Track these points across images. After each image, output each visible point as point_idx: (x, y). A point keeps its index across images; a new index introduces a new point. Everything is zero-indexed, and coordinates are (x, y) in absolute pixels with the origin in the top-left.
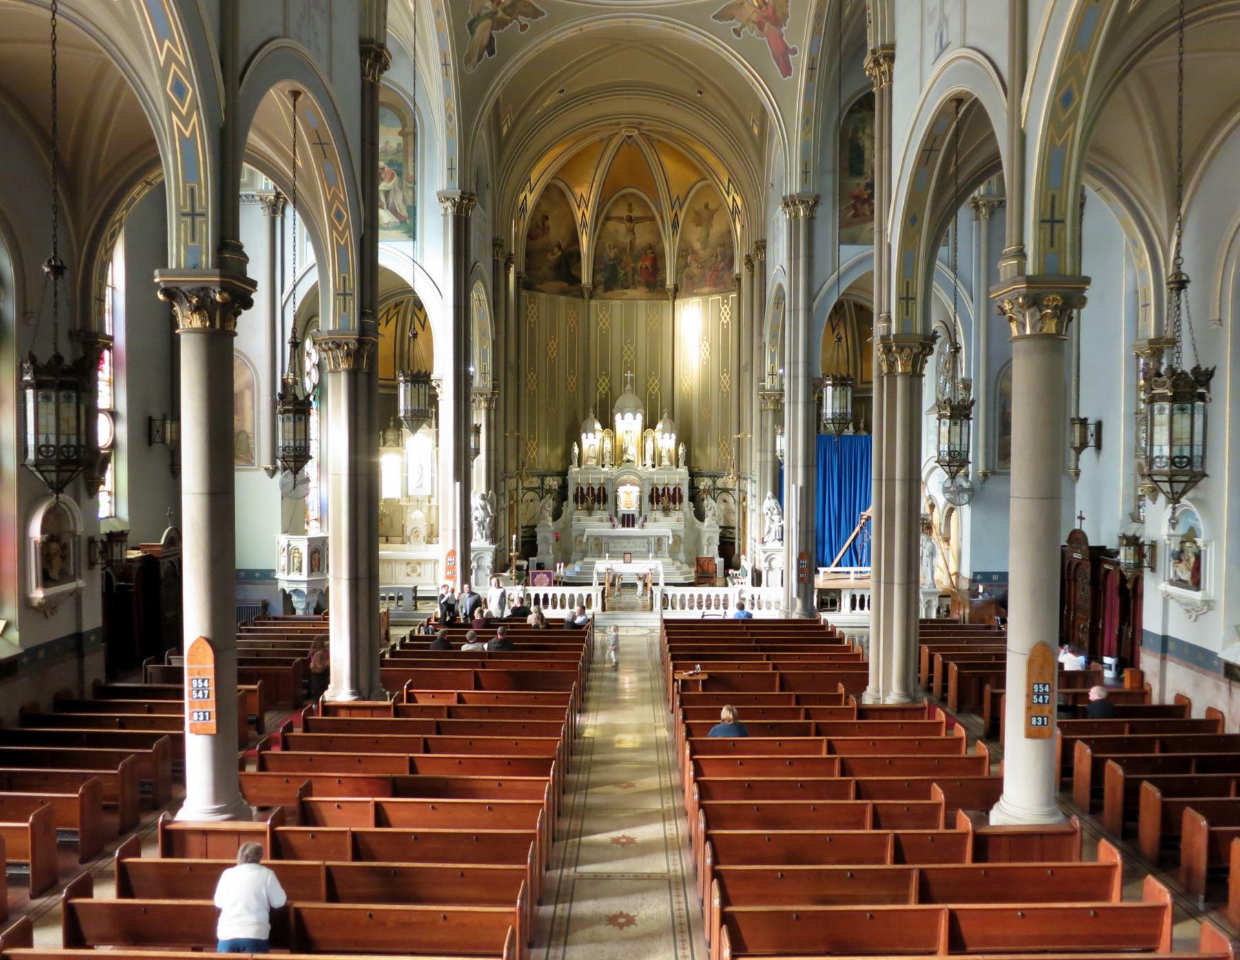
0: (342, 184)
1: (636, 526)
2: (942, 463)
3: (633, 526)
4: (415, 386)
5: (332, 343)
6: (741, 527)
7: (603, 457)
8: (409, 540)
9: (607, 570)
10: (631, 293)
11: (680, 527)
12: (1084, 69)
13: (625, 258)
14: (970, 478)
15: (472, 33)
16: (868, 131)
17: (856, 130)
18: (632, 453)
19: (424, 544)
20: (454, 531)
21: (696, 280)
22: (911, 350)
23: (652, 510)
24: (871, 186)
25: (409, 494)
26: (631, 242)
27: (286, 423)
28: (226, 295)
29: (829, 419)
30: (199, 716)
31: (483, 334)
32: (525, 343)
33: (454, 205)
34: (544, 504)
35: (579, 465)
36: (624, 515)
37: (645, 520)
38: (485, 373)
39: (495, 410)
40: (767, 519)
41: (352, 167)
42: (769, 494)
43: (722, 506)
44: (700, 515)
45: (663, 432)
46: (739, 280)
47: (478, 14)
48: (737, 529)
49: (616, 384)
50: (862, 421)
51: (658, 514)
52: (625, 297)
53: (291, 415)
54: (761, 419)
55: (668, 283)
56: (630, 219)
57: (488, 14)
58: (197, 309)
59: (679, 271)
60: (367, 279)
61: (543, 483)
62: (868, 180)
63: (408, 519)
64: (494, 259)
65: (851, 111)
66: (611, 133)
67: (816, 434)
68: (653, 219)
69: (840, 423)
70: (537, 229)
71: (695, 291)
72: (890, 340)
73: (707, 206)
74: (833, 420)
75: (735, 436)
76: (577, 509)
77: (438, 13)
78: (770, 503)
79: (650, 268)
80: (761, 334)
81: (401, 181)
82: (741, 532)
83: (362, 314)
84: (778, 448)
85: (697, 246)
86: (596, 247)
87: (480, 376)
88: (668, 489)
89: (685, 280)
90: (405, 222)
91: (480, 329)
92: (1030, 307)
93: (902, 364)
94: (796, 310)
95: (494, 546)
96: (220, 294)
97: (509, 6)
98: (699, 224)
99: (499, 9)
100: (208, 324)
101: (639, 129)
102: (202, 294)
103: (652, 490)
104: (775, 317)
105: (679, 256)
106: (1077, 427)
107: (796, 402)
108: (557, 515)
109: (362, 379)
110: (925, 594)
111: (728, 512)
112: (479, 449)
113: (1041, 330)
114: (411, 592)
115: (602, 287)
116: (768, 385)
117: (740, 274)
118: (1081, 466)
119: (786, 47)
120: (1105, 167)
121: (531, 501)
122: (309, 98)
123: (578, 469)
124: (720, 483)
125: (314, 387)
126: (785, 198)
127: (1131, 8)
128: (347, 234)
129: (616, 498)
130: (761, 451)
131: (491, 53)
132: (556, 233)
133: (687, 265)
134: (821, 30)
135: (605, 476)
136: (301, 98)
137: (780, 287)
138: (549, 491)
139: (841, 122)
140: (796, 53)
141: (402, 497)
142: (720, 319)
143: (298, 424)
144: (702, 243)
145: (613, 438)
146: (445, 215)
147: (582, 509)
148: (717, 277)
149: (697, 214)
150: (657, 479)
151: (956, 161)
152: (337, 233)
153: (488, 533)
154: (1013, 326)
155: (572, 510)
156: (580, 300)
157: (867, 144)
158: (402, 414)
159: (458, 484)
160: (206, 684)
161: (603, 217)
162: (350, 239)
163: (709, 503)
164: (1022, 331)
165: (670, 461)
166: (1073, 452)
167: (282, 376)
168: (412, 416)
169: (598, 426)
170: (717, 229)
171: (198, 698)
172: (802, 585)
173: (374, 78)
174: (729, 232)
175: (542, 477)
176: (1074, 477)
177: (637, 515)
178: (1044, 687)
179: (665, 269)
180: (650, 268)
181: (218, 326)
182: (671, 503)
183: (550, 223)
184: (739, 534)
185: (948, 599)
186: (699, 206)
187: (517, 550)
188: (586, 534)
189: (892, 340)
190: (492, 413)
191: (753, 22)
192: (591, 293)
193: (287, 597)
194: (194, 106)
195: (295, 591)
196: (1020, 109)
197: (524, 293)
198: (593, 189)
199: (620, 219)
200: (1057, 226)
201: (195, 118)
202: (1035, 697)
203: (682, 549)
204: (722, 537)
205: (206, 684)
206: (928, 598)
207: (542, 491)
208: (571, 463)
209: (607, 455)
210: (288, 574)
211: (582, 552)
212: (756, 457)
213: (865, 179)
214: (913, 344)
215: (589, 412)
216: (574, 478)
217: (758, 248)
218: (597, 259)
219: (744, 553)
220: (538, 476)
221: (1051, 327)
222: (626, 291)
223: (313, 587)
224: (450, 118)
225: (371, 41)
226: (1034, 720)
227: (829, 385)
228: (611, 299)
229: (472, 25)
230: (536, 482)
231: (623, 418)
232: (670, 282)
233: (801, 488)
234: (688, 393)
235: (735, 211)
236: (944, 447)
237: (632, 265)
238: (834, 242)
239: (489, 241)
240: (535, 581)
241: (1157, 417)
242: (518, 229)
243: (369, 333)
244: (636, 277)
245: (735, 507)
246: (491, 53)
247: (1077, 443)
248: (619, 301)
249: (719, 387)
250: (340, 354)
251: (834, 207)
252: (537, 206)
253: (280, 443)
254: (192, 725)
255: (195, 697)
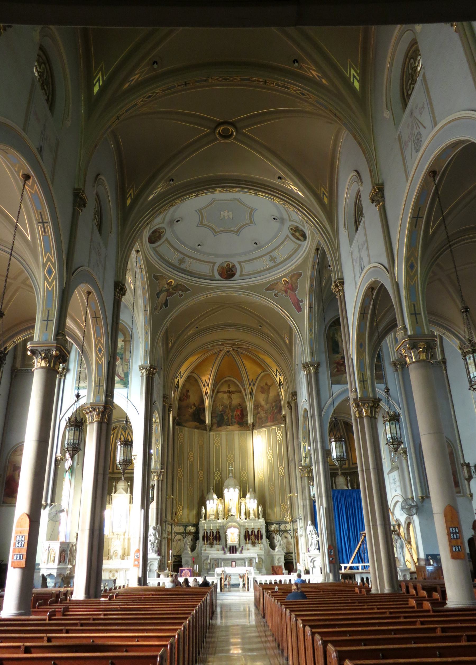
0: (103, 336)
1: (237, 552)
2: (389, 444)
3: (236, 553)
4: (125, 447)
5: (92, 408)
6: (296, 551)
7: (218, 513)
8: (112, 558)
9: (223, 571)
10: (230, 428)
11: (262, 553)
12: (416, 255)
13: (227, 411)
14: (415, 499)
15: (158, 297)
16: (339, 334)
17: (334, 334)
18: (234, 511)
19: (120, 560)
20: (140, 538)
21: (263, 419)
22: (369, 404)
23: (246, 544)
24: (343, 358)
25: (113, 531)
26: (230, 403)
27: (70, 432)
28: (58, 352)
29: (335, 458)
30: (17, 557)
31: (157, 440)
32: (177, 452)
33: (146, 371)
34: (186, 541)
35: (205, 519)
36: (230, 546)
37: (242, 549)
38: (157, 461)
39: (162, 481)
40: (309, 537)
41: (108, 332)
42: (310, 522)
43: (285, 541)
44: (273, 546)
45: (250, 499)
46: (285, 417)
47: (161, 290)
48: (294, 553)
49: (224, 476)
50: (355, 484)
51: (249, 546)
52: (227, 430)
53: (73, 428)
54: (302, 483)
55: (249, 422)
56: (229, 392)
57: (165, 290)
58: (44, 358)
59: (254, 416)
60: (110, 380)
61: (185, 530)
62: (342, 355)
63: (112, 545)
64: (163, 404)
65: (331, 326)
66: (220, 349)
67: (331, 489)
68: (240, 392)
69: (341, 460)
70: (184, 396)
71: (263, 425)
72: (358, 400)
73: (267, 384)
74: (337, 459)
75: (289, 495)
76: (204, 544)
77: (144, 288)
78: (310, 528)
79: (240, 415)
80: (298, 438)
81: (122, 361)
82: (296, 555)
83: (107, 396)
84: (312, 493)
85: (263, 403)
86: (213, 406)
87: (155, 462)
88: (254, 532)
89: (257, 420)
90: (123, 380)
91: (155, 438)
92: (412, 349)
93: (365, 411)
94: (314, 416)
95: (159, 557)
96: (55, 351)
97: (175, 287)
98: (263, 393)
99: (170, 288)
100: (48, 365)
101: (233, 347)
102: (47, 352)
103: (246, 532)
104: (304, 427)
105: (254, 409)
106: (465, 468)
107: (318, 462)
108: (193, 549)
109: (104, 426)
110: (402, 571)
111: (288, 543)
112: (153, 498)
113: (419, 358)
114: (112, 582)
115: (216, 425)
116: (303, 463)
117: (285, 415)
118: (472, 492)
119: (298, 300)
120: (444, 323)
121: (179, 540)
122: (94, 294)
123: (205, 521)
124: (282, 527)
125: (69, 468)
126: (303, 364)
127: (430, 233)
128: (103, 359)
129: (226, 537)
130: (303, 500)
131: (166, 306)
132: (193, 399)
133: (258, 413)
134: (313, 291)
135: (220, 525)
136: (90, 296)
137: (306, 409)
138: (189, 533)
139: (327, 331)
140: (303, 302)
141: (110, 533)
142: (277, 438)
143: (76, 432)
144: (265, 401)
145: (223, 503)
146: (142, 376)
147: (207, 544)
148: (273, 417)
149: (262, 388)
150: (248, 526)
151: (376, 320)
152: (98, 358)
153: (156, 549)
154: (407, 359)
155: (202, 545)
156: (205, 432)
157: (340, 340)
158: (118, 461)
159: (143, 510)
160: (23, 539)
161: (216, 391)
162: (104, 361)
163: (277, 538)
164: (411, 360)
165: (255, 515)
166: (466, 482)
167: (56, 455)
168: (123, 462)
169: (215, 496)
170: (272, 394)
171: (18, 546)
172: (332, 565)
173: (119, 297)
174: (278, 395)
175: (185, 526)
176: (470, 498)
177: (237, 546)
178: (455, 529)
179: (247, 415)
180: (240, 415)
181: (52, 366)
182: (256, 540)
183: (190, 394)
184: (295, 557)
185: (416, 574)
186: (263, 384)
187: (171, 560)
188: (210, 558)
189: (359, 400)
190: (160, 482)
191: (283, 291)
192: (210, 428)
193: (44, 579)
194: (55, 278)
195: (50, 575)
196: (394, 274)
197: (177, 427)
198: (211, 377)
199: (224, 392)
200: (418, 316)
201: (54, 283)
202: (452, 535)
203: (264, 566)
204: (286, 559)
205: (23, 539)
206: (404, 574)
207: (185, 533)
208: (201, 518)
209: (221, 513)
210: (47, 564)
211: (207, 570)
212: (301, 503)
213: (341, 355)
214: (369, 402)
215: (210, 489)
216: (203, 527)
217: (293, 396)
218: (213, 412)
219: (299, 562)
220: (183, 526)
221: (423, 356)
222: (228, 427)
223: (60, 572)
224: (147, 333)
225: (119, 282)
226: (454, 548)
227: (333, 441)
228: (221, 431)
229: (158, 295)
230: (182, 529)
231: (228, 491)
232: (250, 422)
233: (325, 508)
234: (262, 479)
235: (281, 384)
236: (389, 436)
237: (231, 414)
238: (329, 384)
239: (162, 395)
240: (182, 574)
241: (469, 361)
242: (174, 395)
243: (109, 403)
244: (233, 420)
245: (291, 541)
246: (166, 306)
247: (467, 476)
248: (225, 432)
249: (279, 474)
250: (95, 413)
251: (327, 367)
252: (184, 385)
253: (66, 442)
254: (13, 562)
255: (17, 546)
